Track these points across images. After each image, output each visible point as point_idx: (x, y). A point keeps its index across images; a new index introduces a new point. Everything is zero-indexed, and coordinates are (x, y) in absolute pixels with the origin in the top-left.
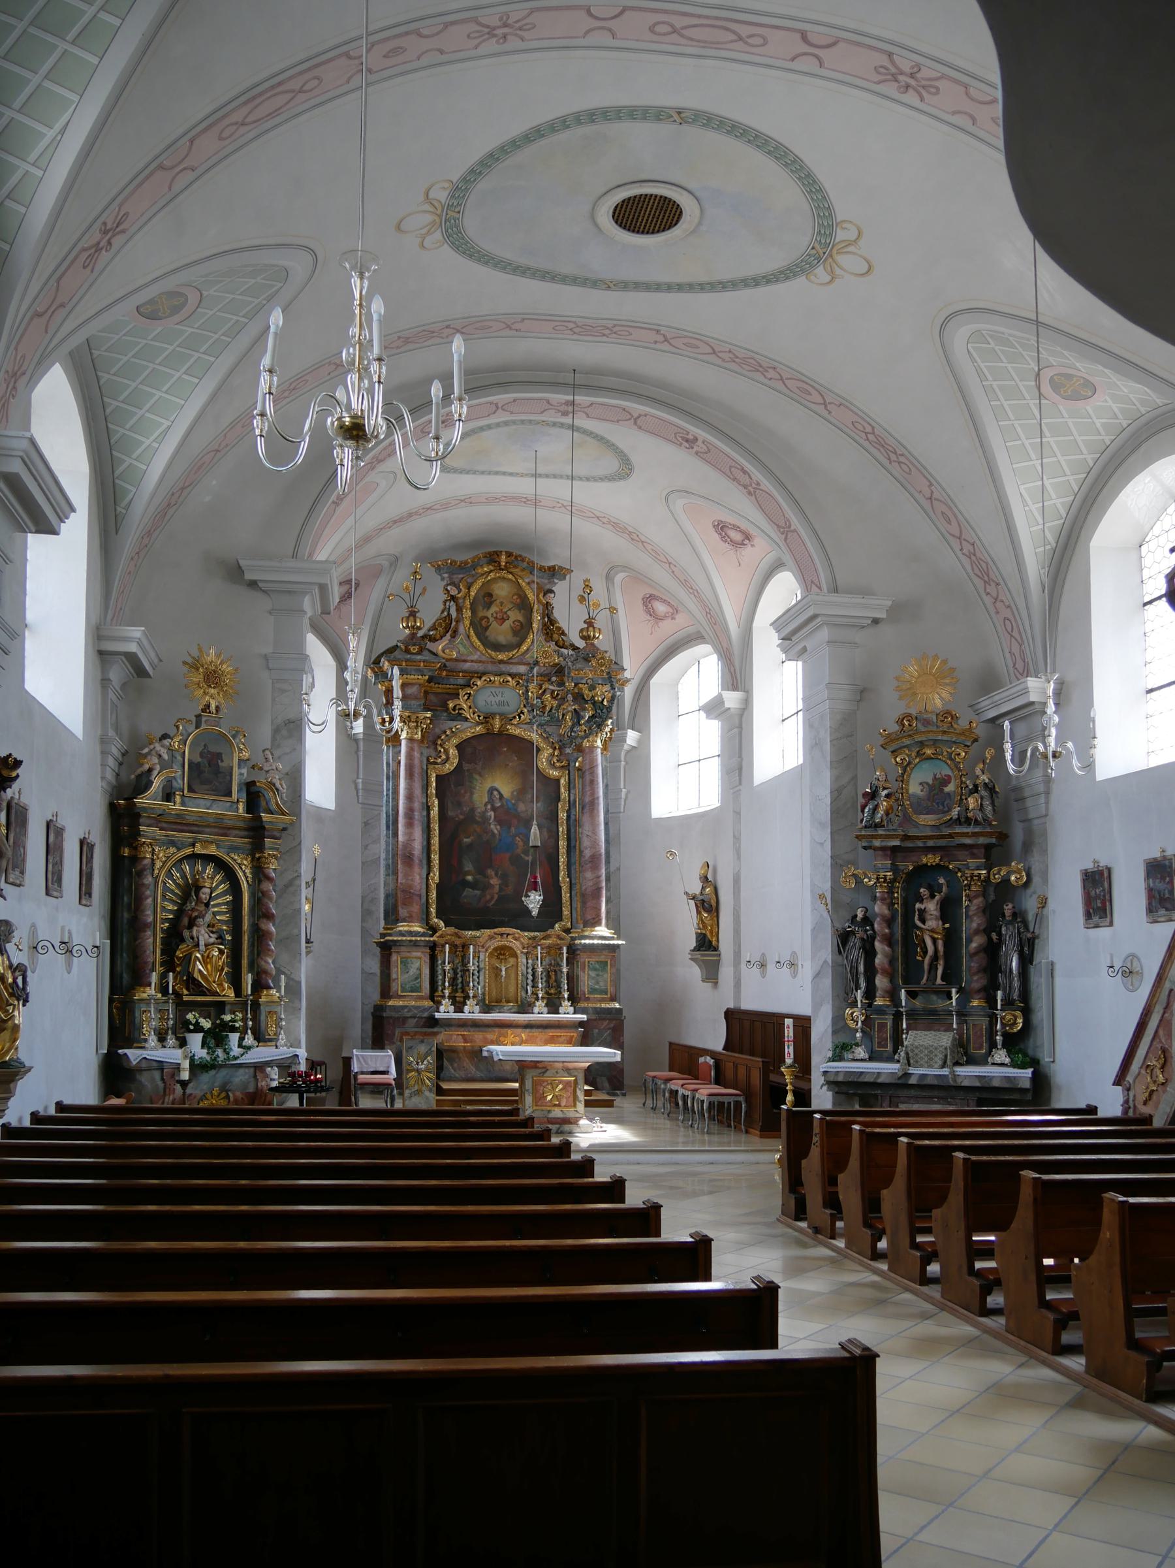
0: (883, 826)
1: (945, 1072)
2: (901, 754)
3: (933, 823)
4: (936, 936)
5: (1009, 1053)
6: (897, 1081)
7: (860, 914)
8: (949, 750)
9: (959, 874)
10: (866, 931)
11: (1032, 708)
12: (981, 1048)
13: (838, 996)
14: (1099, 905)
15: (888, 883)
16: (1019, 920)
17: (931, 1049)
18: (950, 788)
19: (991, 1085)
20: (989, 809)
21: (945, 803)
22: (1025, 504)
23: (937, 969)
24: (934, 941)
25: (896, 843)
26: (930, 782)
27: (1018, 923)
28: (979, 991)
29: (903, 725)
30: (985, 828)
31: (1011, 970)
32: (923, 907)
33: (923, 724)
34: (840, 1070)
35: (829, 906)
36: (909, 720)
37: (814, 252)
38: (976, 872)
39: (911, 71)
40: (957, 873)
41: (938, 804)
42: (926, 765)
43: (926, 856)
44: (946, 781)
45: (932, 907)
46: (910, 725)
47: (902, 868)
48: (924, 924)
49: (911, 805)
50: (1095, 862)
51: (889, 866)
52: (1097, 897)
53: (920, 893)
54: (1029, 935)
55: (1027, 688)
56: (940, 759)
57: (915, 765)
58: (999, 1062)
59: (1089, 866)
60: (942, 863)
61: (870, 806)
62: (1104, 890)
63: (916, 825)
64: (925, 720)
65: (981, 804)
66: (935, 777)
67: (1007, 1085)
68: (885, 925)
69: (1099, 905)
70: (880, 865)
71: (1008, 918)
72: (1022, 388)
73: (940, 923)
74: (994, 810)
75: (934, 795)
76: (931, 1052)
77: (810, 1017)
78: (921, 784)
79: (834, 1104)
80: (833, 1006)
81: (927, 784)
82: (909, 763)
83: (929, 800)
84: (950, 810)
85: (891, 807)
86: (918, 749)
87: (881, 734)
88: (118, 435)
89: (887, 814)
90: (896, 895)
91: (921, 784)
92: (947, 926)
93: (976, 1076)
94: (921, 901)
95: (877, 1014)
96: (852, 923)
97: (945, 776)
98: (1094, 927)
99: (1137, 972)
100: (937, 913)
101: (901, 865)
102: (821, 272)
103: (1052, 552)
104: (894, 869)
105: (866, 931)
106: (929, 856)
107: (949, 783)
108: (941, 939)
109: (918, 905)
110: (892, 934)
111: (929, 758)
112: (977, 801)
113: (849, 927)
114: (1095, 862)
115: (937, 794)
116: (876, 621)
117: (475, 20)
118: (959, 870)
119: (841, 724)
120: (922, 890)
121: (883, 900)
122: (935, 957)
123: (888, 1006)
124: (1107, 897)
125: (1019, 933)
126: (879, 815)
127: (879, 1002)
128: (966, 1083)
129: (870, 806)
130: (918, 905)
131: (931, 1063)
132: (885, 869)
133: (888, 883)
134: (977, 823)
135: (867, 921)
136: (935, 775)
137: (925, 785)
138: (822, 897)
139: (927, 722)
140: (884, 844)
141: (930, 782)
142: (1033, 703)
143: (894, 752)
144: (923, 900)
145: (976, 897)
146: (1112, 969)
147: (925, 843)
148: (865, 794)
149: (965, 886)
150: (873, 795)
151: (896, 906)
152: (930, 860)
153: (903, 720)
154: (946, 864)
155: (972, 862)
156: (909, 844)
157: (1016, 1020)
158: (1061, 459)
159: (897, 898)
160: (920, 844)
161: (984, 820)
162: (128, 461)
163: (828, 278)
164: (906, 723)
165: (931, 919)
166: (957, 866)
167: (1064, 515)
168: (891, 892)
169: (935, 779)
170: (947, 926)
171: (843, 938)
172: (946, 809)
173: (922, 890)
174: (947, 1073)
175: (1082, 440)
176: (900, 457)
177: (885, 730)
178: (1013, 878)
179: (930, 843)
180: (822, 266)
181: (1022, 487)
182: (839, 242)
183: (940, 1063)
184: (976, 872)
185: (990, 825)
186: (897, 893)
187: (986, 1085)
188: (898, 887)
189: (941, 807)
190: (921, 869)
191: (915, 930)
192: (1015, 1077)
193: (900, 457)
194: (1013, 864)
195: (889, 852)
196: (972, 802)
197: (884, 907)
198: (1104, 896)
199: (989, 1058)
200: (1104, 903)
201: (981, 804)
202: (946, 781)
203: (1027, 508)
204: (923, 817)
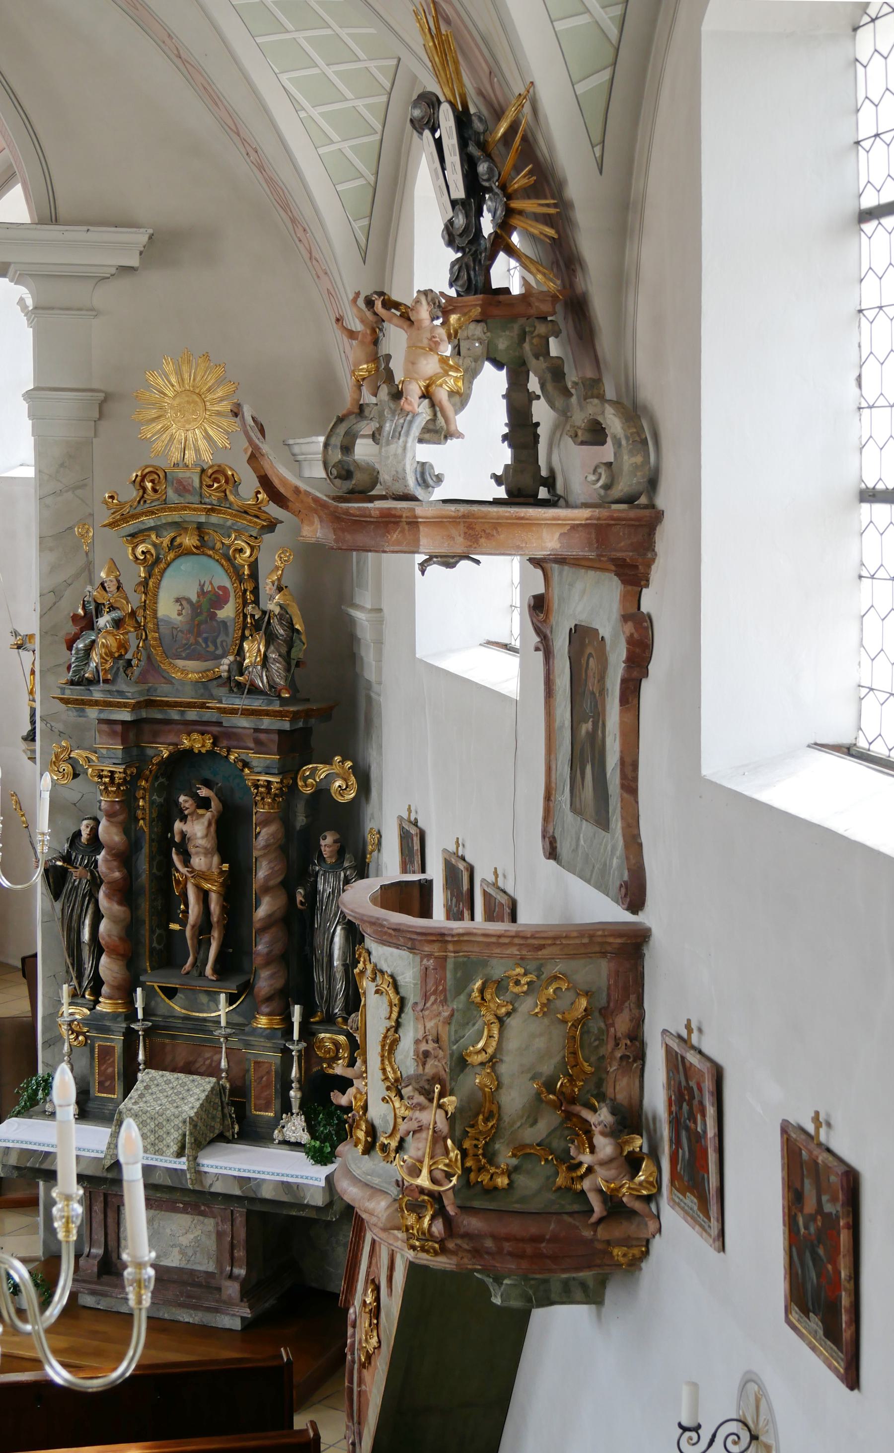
1: (182, 1164)
2: (143, 541)
4: (207, 886)
5: (311, 1128)
6: (105, 1174)
8: (226, 542)
12: (267, 1108)
16: (346, 864)
17: (160, 1119)
18: (227, 612)
19: (259, 1196)
20: (277, 668)
21: (219, 641)
22: (297, 107)
23: (210, 944)
24: (204, 896)
26: (194, 598)
27: (345, 869)
28: (269, 999)
29: (144, 489)
30: (270, 703)
31: (331, 956)
33: (176, 491)
34: (10, 1145)
36: (152, 481)
40: (242, 770)
41: (206, 640)
42: (185, 565)
43: (189, 734)
44: (218, 599)
46: (155, 490)
53: (177, 804)
56: (210, 556)
57: (168, 565)
58: (293, 1140)
63: (169, 681)
64: (180, 482)
66: (202, 589)
67: (285, 1198)
70: (104, 751)
71: (329, 861)
73: (216, 859)
75: (199, 625)
76: (160, 1125)
78: (178, 600)
81: (189, 601)
82: (157, 561)
83: (190, 631)
86: (172, 534)
87: (106, 503)
91: (178, 600)
93: (235, 1177)
94: (184, 819)
97: (220, 588)
103: (371, 190)
107: (226, 602)
108: (214, 891)
111: (188, 553)
115: (206, 622)
116: (126, 270)
119: (62, 465)
120: (182, 799)
122: (204, 926)
126: (93, 665)
128: (218, 1188)
130: (178, 825)
131: (161, 1146)
134: (253, 690)
136: (202, 586)
137: (184, 603)
139: (182, 488)
141: (194, 598)
143: (134, 537)
144: (186, 817)
147: (183, 713)
148: (75, 618)
150: (87, 622)
152: (198, 743)
153: (142, 480)
157: (338, 1051)
164: (149, 485)
165: (197, 853)
166: (243, 757)
167: (379, 127)
169: (202, 593)
170: (225, 867)
174: (185, 1167)
177: (112, 497)
178: (337, 784)
181: (284, 78)
183: (174, 1148)
186: (144, 798)
187: (252, 1195)
188: (144, 789)
189: (211, 648)
192: (298, 1185)
195: (119, 728)
196: (253, 649)
199: (276, 1132)
202: (218, 599)
203: (303, 114)
204: (180, 663)
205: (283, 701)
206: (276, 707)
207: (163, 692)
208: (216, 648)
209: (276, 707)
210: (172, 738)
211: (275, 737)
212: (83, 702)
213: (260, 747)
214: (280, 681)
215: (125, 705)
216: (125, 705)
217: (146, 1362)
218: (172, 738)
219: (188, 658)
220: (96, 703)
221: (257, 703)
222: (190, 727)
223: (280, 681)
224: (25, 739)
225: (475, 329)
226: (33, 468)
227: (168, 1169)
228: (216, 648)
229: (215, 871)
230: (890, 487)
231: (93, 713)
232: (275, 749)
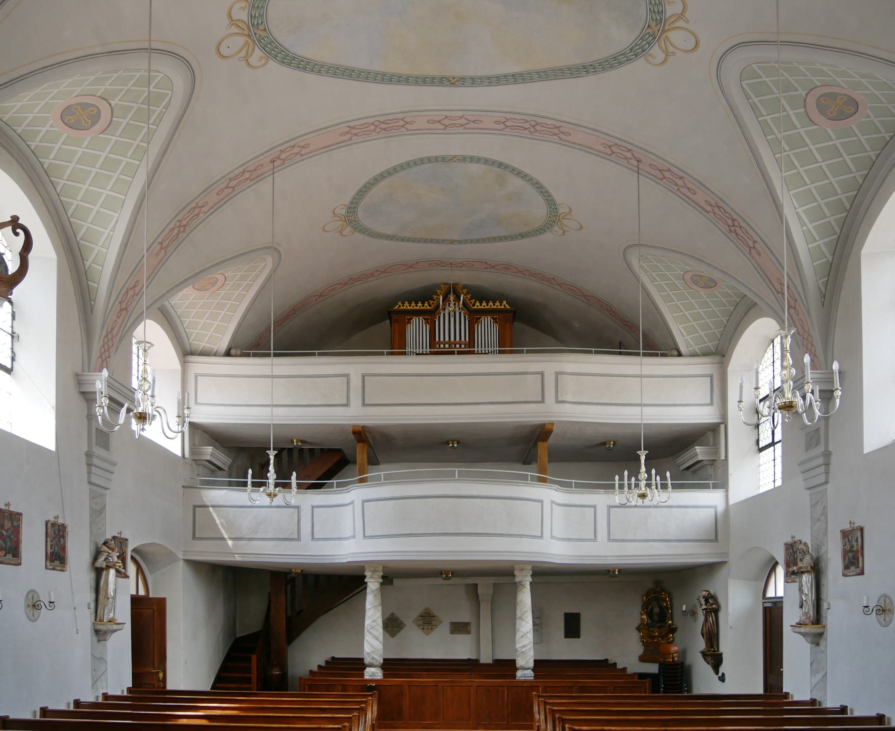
11: (701, 463)
37: (650, 30)
39: (607, 147)
50: (793, 537)
55: (696, 453)
59: (789, 540)
72: (672, 295)
88: (73, 207)
98: (791, 582)
99: (889, 610)
102: (656, 51)
114: (793, 537)
117: (408, 130)
142: (702, 461)
146: (866, 608)
158: (833, 180)
162: (97, 248)
163: (662, 56)
167: (838, 230)
175: (865, 139)
176: (711, 210)
180: (657, 44)
182: (670, 17)
193: (711, 210)
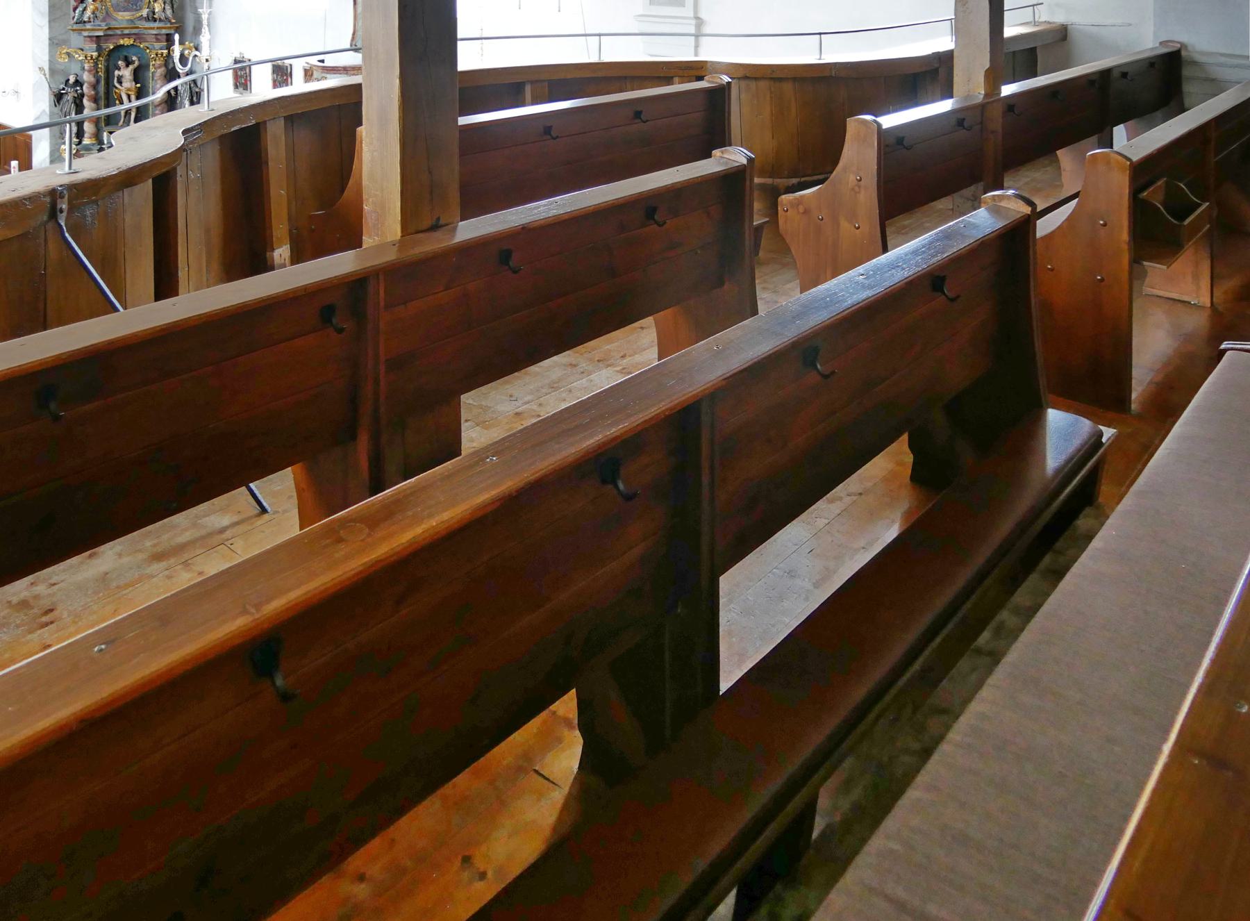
0: (90, 22)
3: (129, 18)
4: (130, 93)
7: (72, 80)
9: (148, 51)
10: (77, 91)
13: (55, 136)
14: (243, 81)
15: (94, 60)
21: (138, 5)
25: (101, 33)
30: (166, 24)
32: (121, 73)
35: (48, 76)
38: (160, 52)
41: (132, 4)
45: (127, 73)
47: (104, 47)
48: (121, 85)
49: (112, 6)
50: (241, 53)
51: (95, 48)
52: (241, 77)
54: (197, 90)
60: (135, 44)
61: (80, 9)
62: (246, 73)
63: (115, 20)
65: (164, 8)
68: (91, 89)
69: (243, 81)
73: (134, 83)
74: (173, 12)
77: (31, 168)
79: (50, 119)
80: (51, 143)
84: (141, 9)
85: (97, 9)
89: (93, 13)
90: (100, 66)
92: (138, 85)
94: (119, 69)
95: (86, 150)
96: (66, 85)
100: (131, 78)
101: (104, 46)
104: (99, 49)
105: (77, 91)
106: (126, 39)
109: (117, 73)
110: (97, 93)
112: (161, 6)
113: (64, 89)
114: (241, 53)
118: (148, 48)
120: (120, 62)
121: (90, 71)
123: (93, 145)
124: (248, 78)
125: (190, 88)
127: (86, 141)
129: (80, 9)
130: (117, 73)
132: (90, 49)
133: (94, 60)
135: (78, 83)
138: (41, 69)
140: (91, 34)
145: (159, 67)
149: (153, 58)
151: (100, 73)
152: (126, 42)
154: (139, 44)
155: (157, 45)
156: (110, 32)
159: (101, 68)
160: (118, 32)
161: (166, 19)
168: (96, 64)
170: (138, 85)
171: (58, 97)
172: (138, 8)
173: (120, 62)
179: (126, 32)
184: (160, 52)
185: (170, 21)
189: (135, 7)
190: (118, 48)
191: (114, 89)
194: (187, 43)
195: (94, 39)
197: (91, 76)
198: (246, 76)
200: (246, 80)
201: (164, 8)
204: (121, 13)
205: (172, 23)
206: (169, 25)
207: (114, 24)
208: (137, 7)
209: (169, 25)
210: (115, 41)
211: (165, 37)
212: (82, 30)
213: (158, 40)
214: (170, 16)
215: (101, 30)
216: (101, 30)
217: (1186, 72)
218: (115, 41)
219: (124, 11)
220: (88, 30)
221: (161, 25)
222: (123, 36)
223: (170, 16)
224: (235, 60)
225: (985, 203)
226: (459, 36)
227: (1229, 89)
228: (137, 7)
229: (133, 87)
230: (947, 10)
231: (86, 34)
232: (165, 40)
